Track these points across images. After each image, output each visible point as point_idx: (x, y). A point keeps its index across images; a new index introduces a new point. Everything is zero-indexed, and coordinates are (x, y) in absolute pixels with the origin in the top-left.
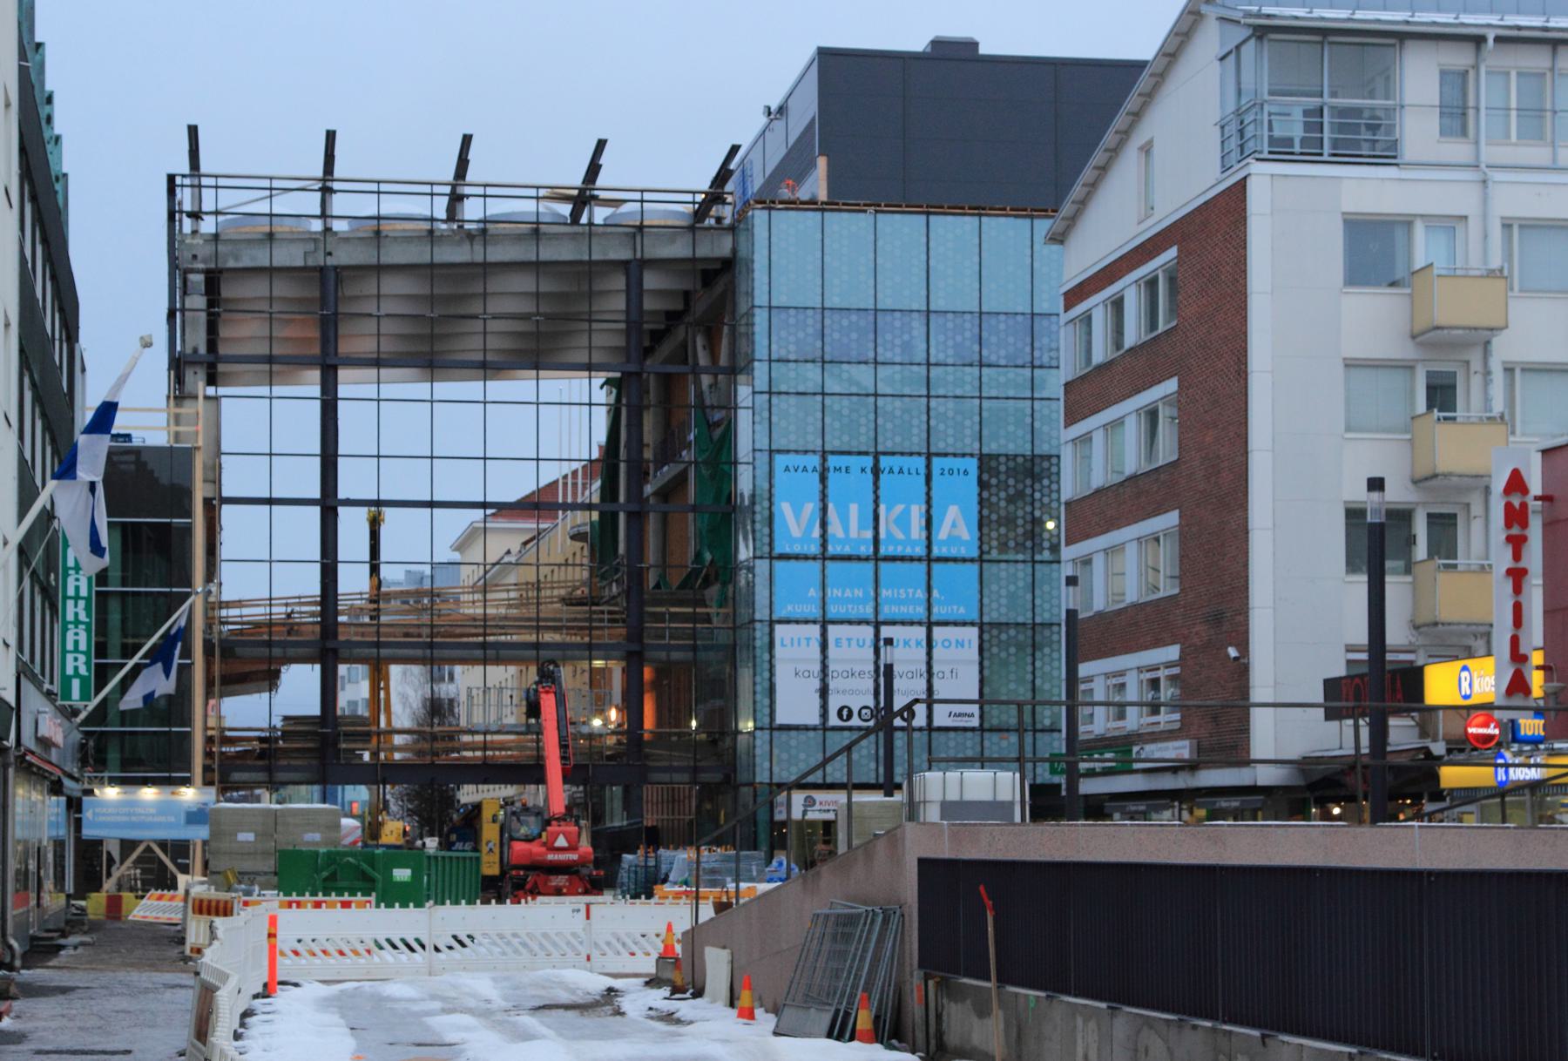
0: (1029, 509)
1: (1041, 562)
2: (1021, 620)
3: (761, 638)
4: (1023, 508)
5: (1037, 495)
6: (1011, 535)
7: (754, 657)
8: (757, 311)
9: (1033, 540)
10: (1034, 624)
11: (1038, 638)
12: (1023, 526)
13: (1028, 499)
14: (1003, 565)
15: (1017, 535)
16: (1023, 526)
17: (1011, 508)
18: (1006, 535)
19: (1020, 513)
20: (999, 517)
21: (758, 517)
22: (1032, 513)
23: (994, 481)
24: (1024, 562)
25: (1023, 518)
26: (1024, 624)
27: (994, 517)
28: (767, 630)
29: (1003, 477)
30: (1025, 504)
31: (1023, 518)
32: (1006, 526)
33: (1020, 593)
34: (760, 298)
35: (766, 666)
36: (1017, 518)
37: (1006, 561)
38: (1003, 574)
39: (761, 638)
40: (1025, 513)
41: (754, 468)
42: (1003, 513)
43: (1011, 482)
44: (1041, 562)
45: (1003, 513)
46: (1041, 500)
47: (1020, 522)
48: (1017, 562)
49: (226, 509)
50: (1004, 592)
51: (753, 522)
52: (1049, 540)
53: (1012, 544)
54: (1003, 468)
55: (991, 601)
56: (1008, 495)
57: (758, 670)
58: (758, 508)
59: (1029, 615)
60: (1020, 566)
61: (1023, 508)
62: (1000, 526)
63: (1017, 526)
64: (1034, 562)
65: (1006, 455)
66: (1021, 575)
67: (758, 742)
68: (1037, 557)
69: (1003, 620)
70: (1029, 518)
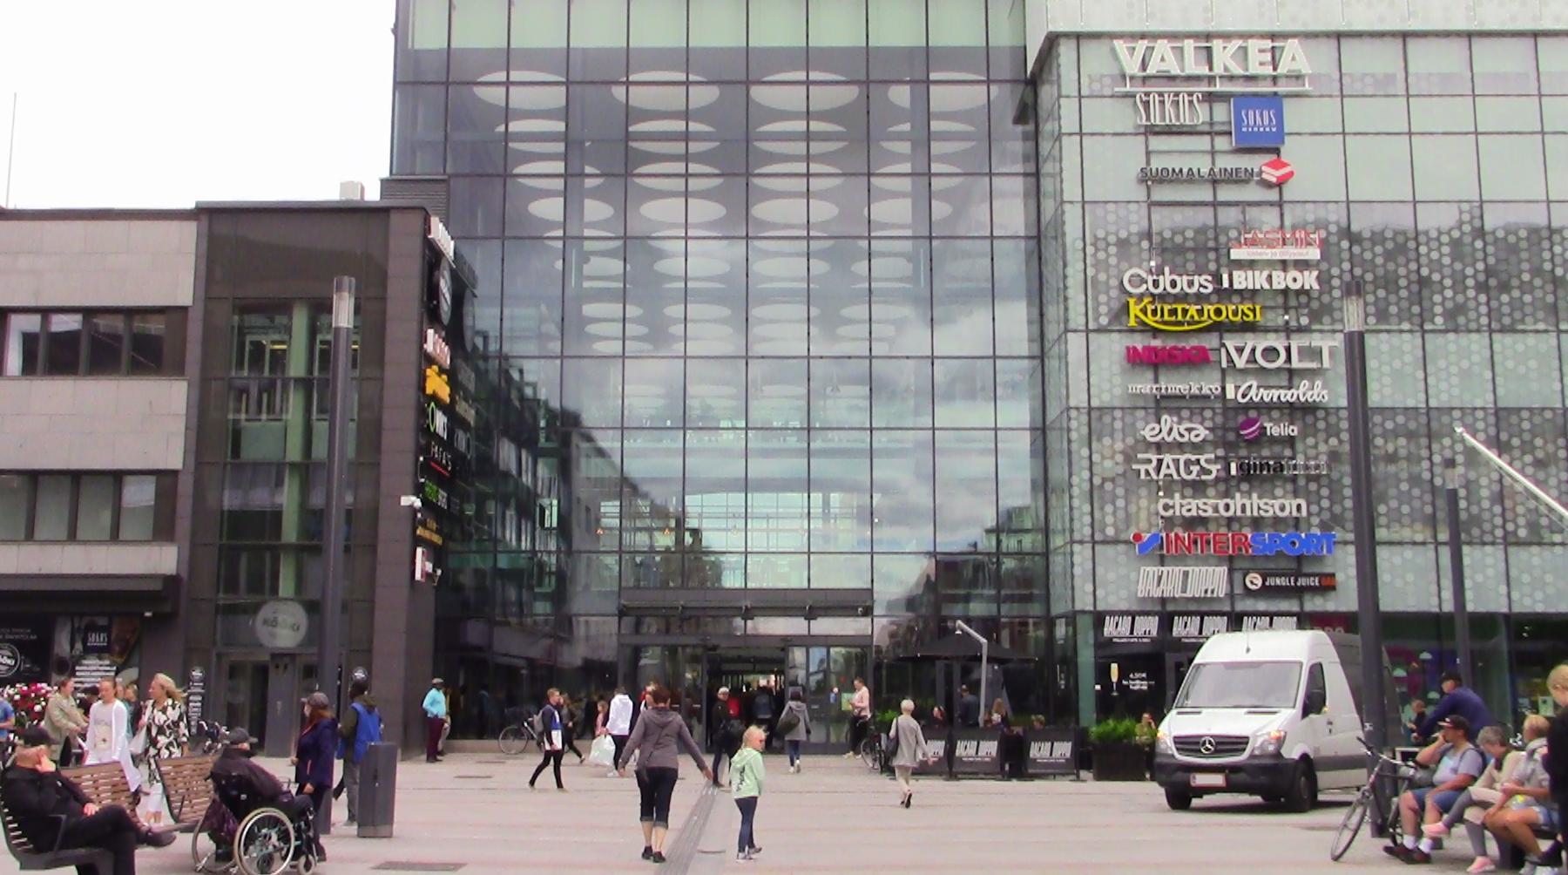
0: (1413, 266)
1: (1432, 331)
2: (1411, 403)
3: (1081, 564)
4: (1406, 265)
5: (1423, 249)
6: (1393, 298)
7: (1066, 299)
8: (1067, 207)
9: (1420, 304)
10: (1429, 409)
11: (1434, 425)
12: (1407, 288)
13: (1412, 255)
14: (1383, 336)
15: (1400, 299)
16: (1407, 288)
17: (1391, 266)
18: (1386, 299)
19: (1402, 271)
20: (1376, 278)
21: (1076, 491)
22: (1418, 271)
23: (1516, 442)
24: (1410, 331)
25: (1406, 277)
26: (1416, 409)
27: (1369, 277)
28: (1084, 418)
29: (1527, 437)
30: (1559, 471)
31: (1406, 277)
32: (1385, 288)
33: (1409, 370)
34: (1071, 191)
35: (1086, 463)
36: (1399, 277)
37: (1388, 331)
38: (1385, 348)
39: (1077, 430)
40: (1409, 272)
41: (1066, 320)
42: (1380, 272)
43: (1539, 442)
44: (1432, 331)
45: (1380, 272)
46: (1428, 254)
47: (1403, 282)
48: (1401, 331)
49: (685, 88)
50: (1386, 369)
51: (1071, 497)
52: (1393, 239)
53: (1393, 309)
54: (1526, 425)
55: (1438, 380)
56: (1386, 250)
57: (1075, 468)
58: (1075, 480)
59: (1422, 396)
60: (1406, 336)
61: (1406, 265)
62: (1377, 288)
63: (1399, 288)
64: (1424, 332)
65: (1530, 409)
66: (1407, 347)
67: (1077, 559)
68: (1428, 326)
69: (1388, 403)
70: (1414, 277)
